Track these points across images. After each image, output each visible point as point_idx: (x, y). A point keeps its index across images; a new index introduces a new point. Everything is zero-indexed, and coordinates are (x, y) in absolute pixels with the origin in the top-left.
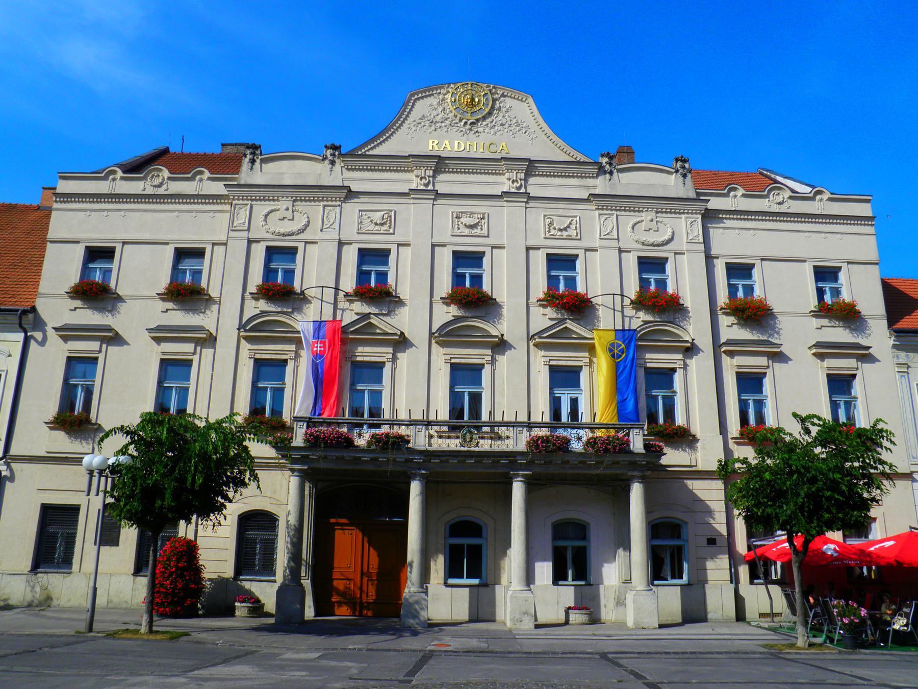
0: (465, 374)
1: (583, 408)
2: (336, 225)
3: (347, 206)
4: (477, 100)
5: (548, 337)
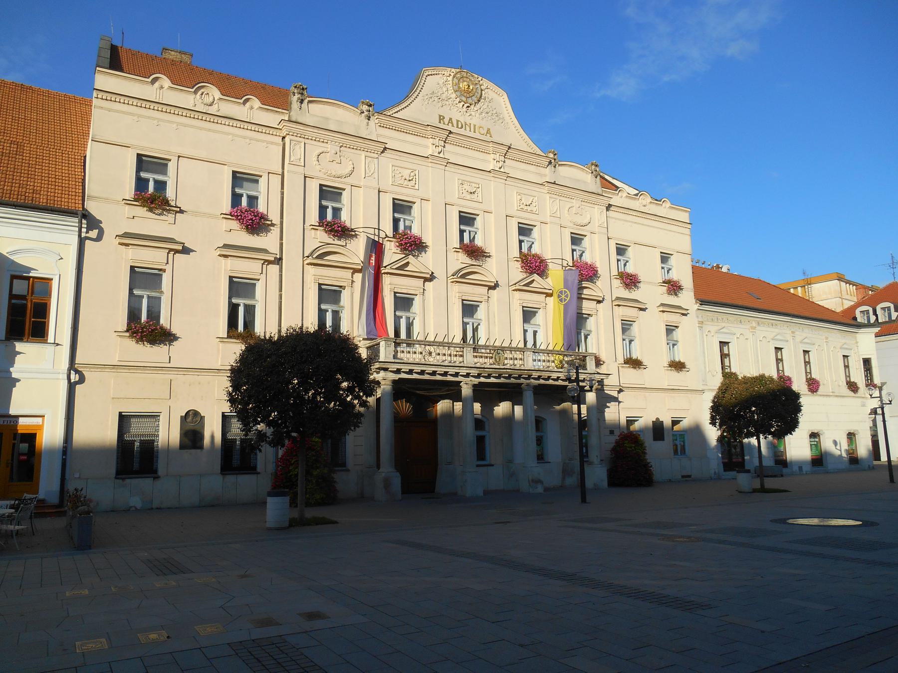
1: (540, 338)
2: (376, 175)
5: (396, 269)
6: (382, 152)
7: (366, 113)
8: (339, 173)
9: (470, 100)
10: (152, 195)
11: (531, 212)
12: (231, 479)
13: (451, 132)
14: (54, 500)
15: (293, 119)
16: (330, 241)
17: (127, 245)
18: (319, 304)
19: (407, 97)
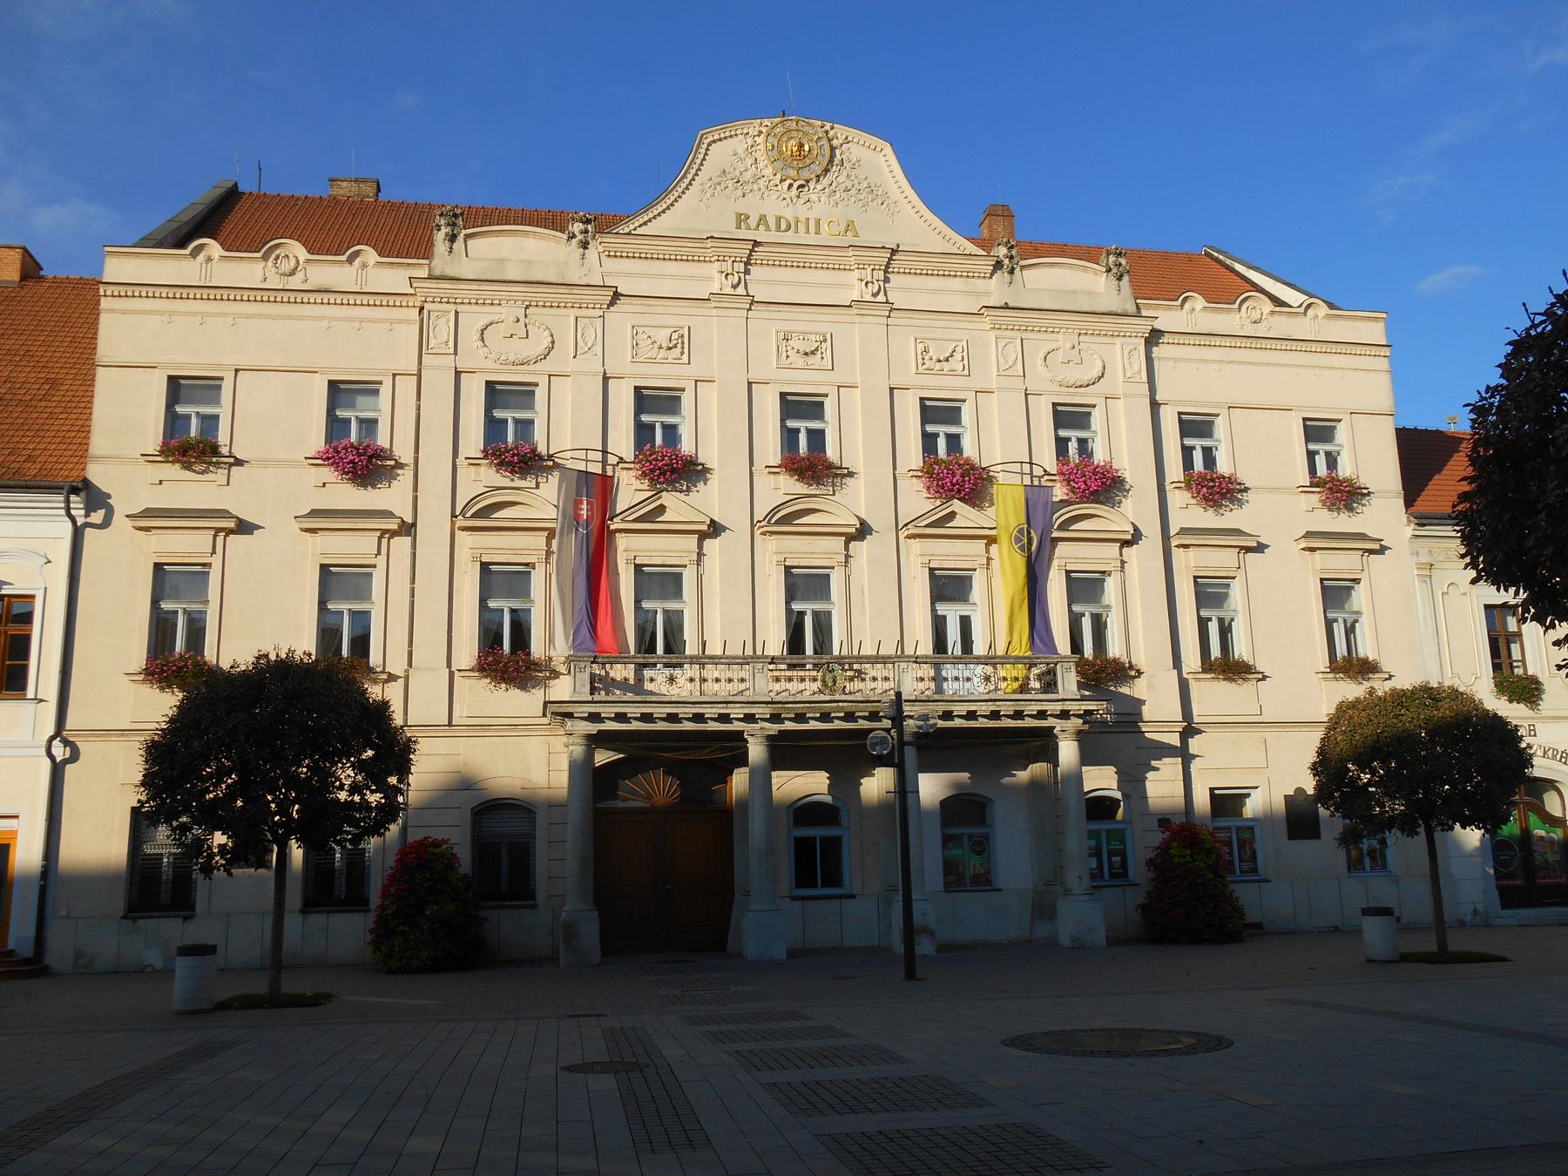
0: (804, 584)
3: (613, 316)
4: (806, 148)
5: (635, 521)
6: (612, 304)
7: (580, 237)
8: (1086, 378)
9: (806, 174)
10: (192, 446)
11: (953, 373)
12: (317, 920)
13: (756, 243)
14: (27, 951)
15: (437, 272)
16: (506, 482)
17: (147, 529)
18: (788, 603)
19: (667, 191)
